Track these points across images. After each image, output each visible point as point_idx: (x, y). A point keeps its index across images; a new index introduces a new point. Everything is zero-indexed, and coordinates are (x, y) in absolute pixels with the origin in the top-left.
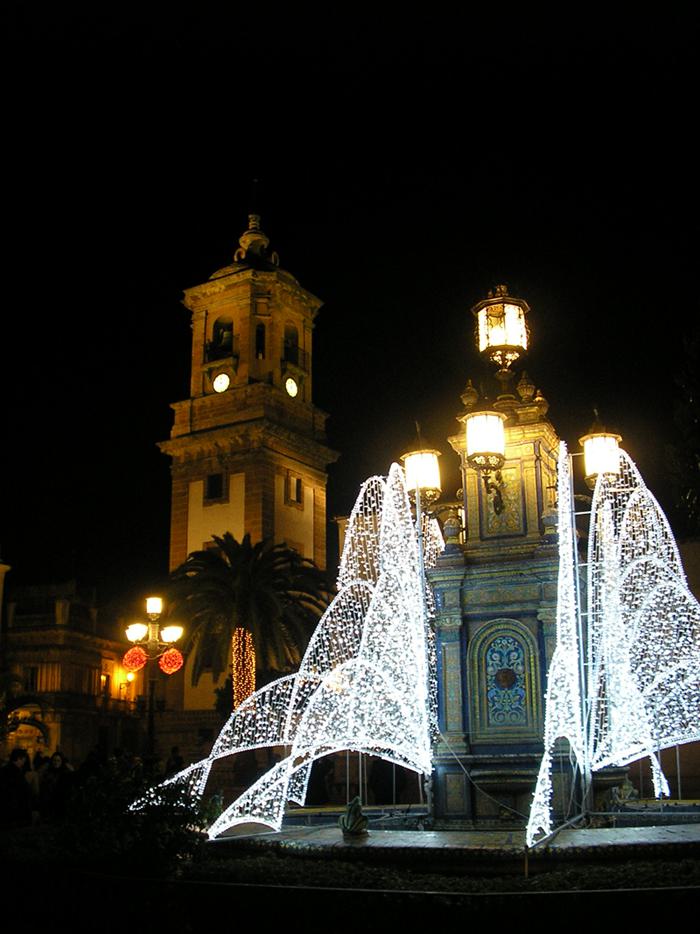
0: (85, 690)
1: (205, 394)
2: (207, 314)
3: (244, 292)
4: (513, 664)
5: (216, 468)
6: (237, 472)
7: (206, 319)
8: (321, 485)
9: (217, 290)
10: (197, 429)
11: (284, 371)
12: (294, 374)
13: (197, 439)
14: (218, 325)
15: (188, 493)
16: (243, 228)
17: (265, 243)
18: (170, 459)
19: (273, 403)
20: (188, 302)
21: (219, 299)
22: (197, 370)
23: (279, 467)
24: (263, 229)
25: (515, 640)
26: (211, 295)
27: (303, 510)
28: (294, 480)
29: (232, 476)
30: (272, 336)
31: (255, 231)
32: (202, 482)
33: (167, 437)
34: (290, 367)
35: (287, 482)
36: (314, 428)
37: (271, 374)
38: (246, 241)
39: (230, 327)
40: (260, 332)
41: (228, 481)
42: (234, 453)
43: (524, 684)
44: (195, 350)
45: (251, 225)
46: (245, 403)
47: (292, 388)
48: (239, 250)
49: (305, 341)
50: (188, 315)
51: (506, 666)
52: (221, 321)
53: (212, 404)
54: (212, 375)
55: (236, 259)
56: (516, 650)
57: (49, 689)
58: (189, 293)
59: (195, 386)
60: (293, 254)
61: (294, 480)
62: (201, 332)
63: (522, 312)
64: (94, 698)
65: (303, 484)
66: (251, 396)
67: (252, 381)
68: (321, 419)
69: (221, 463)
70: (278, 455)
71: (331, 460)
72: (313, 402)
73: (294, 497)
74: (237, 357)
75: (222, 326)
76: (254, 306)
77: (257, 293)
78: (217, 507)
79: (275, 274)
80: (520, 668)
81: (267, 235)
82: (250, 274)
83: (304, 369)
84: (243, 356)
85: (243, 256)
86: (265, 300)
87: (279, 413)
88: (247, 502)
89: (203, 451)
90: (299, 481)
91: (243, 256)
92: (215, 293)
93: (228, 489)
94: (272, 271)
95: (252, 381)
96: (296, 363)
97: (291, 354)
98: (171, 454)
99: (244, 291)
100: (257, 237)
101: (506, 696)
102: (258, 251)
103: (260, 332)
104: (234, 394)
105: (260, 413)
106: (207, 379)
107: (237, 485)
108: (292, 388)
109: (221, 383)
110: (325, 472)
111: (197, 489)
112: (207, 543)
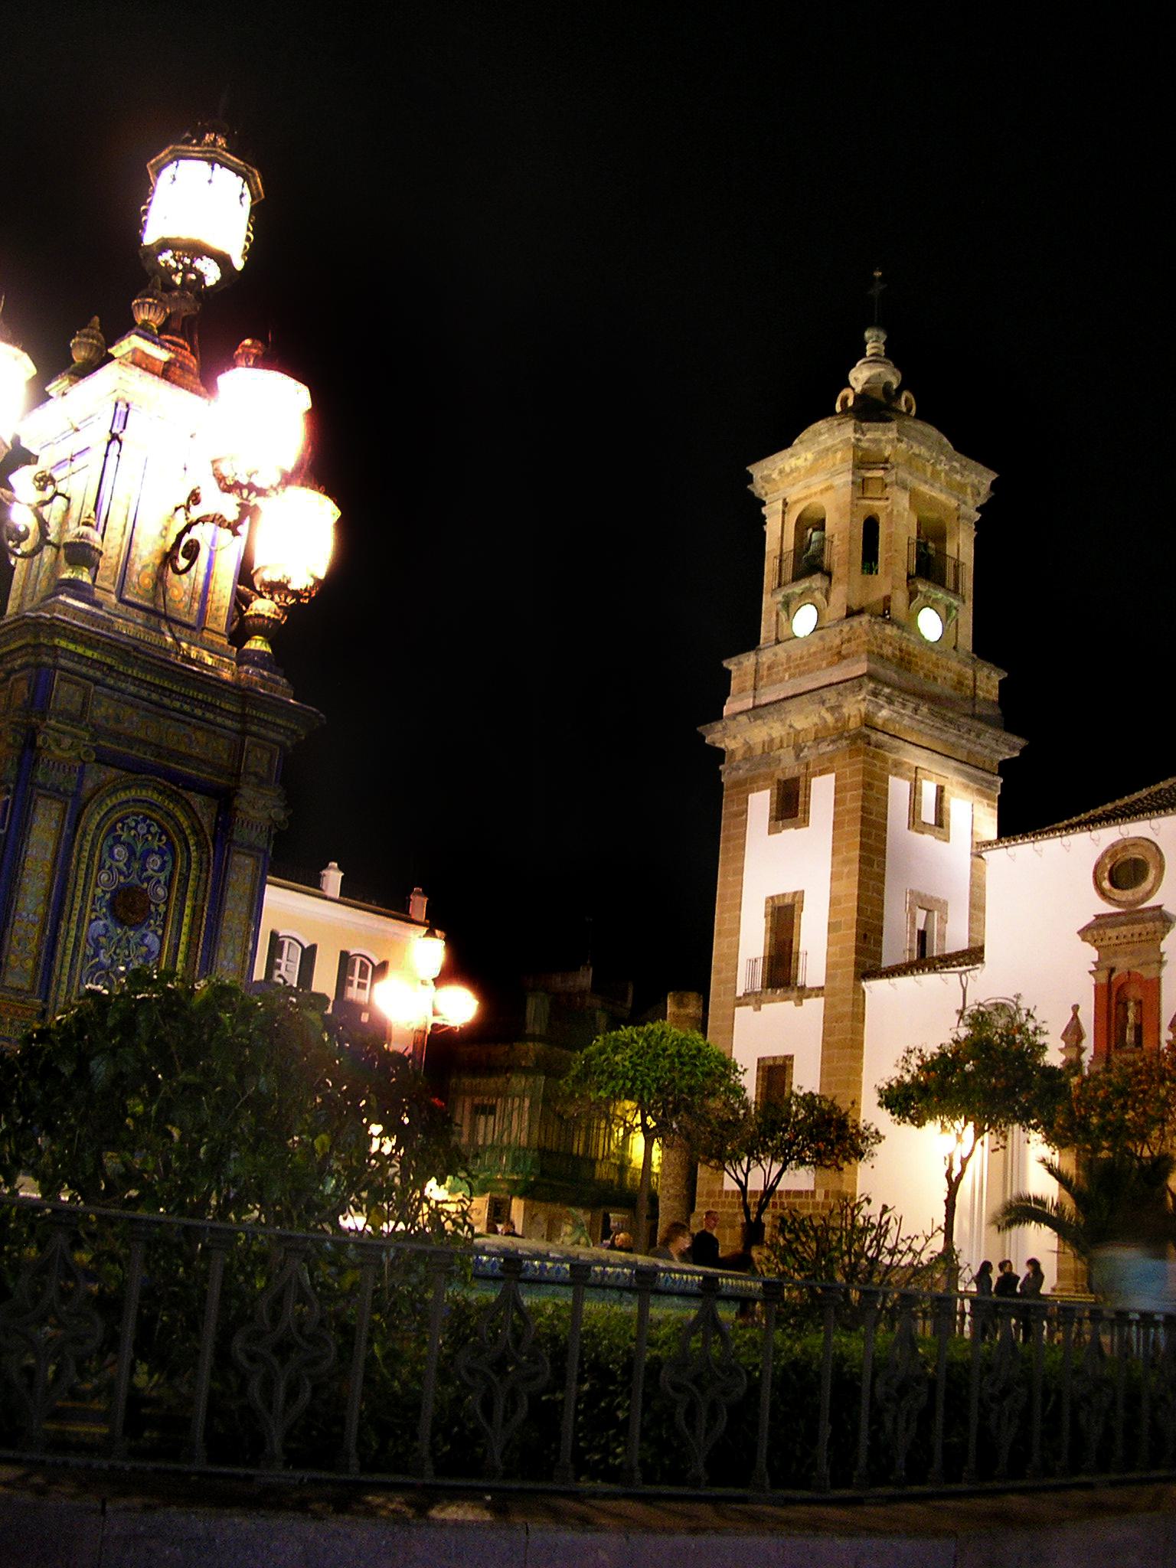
0: (578, 1148)
1: (778, 642)
2: (785, 504)
3: (842, 459)
4: (149, 879)
5: (788, 765)
6: (822, 773)
7: (784, 513)
8: (988, 797)
9: (800, 462)
10: (764, 700)
11: (912, 595)
12: (936, 601)
13: (761, 717)
14: (802, 524)
15: (746, 811)
16: (857, 352)
17: (895, 380)
18: (719, 755)
19: (887, 650)
20: (758, 488)
21: (804, 479)
22: (770, 602)
23: (898, 764)
24: (893, 354)
25: (164, 832)
26: (792, 471)
27: (947, 840)
28: (929, 790)
29: (813, 780)
30: (890, 535)
31: (876, 360)
32: (767, 792)
33: (718, 716)
34: (922, 587)
35: (915, 791)
36: (975, 695)
37: (887, 599)
38: (860, 376)
39: (820, 525)
40: (871, 527)
41: (808, 787)
42: (817, 740)
43: (164, 928)
44: (770, 565)
45: (870, 349)
46: (839, 653)
47: (930, 624)
48: (845, 392)
49: (962, 547)
50: (752, 512)
51: (134, 879)
52: (808, 514)
53: (789, 658)
54: (788, 606)
55: (838, 409)
56: (161, 853)
57: (561, 1149)
58: (758, 470)
59: (766, 631)
60: (949, 399)
61: (929, 790)
62: (778, 534)
63: (246, 190)
64: (593, 1162)
65: (946, 794)
66: (849, 640)
67: (851, 613)
68: (989, 681)
69: (797, 757)
70: (898, 743)
71: (1007, 754)
72: (974, 651)
73: (928, 815)
74: (829, 574)
75: (811, 523)
76: (861, 486)
77: (863, 461)
78: (790, 834)
79: (894, 425)
80: (161, 892)
81: (898, 365)
82: (851, 429)
83: (956, 591)
84: (838, 571)
85: (850, 403)
86: (880, 473)
87: (899, 672)
88: (837, 825)
89: (772, 740)
90: (940, 790)
91: (850, 403)
92: (797, 468)
93: (807, 803)
94: (889, 420)
95: (851, 613)
96: (940, 582)
97: (928, 566)
98: (722, 746)
99: (843, 460)
100: (878, 369)
101: (124, 942)
102: (878, 394)
103: (871, 527)
104: (822, 638)
105: (861, 668)
106: (783, 615)
107: (822, 792)
108: (930, 624)
109: (804, 621)
110: (999, 775)
111: (760, 803)
112: (772, 898)
